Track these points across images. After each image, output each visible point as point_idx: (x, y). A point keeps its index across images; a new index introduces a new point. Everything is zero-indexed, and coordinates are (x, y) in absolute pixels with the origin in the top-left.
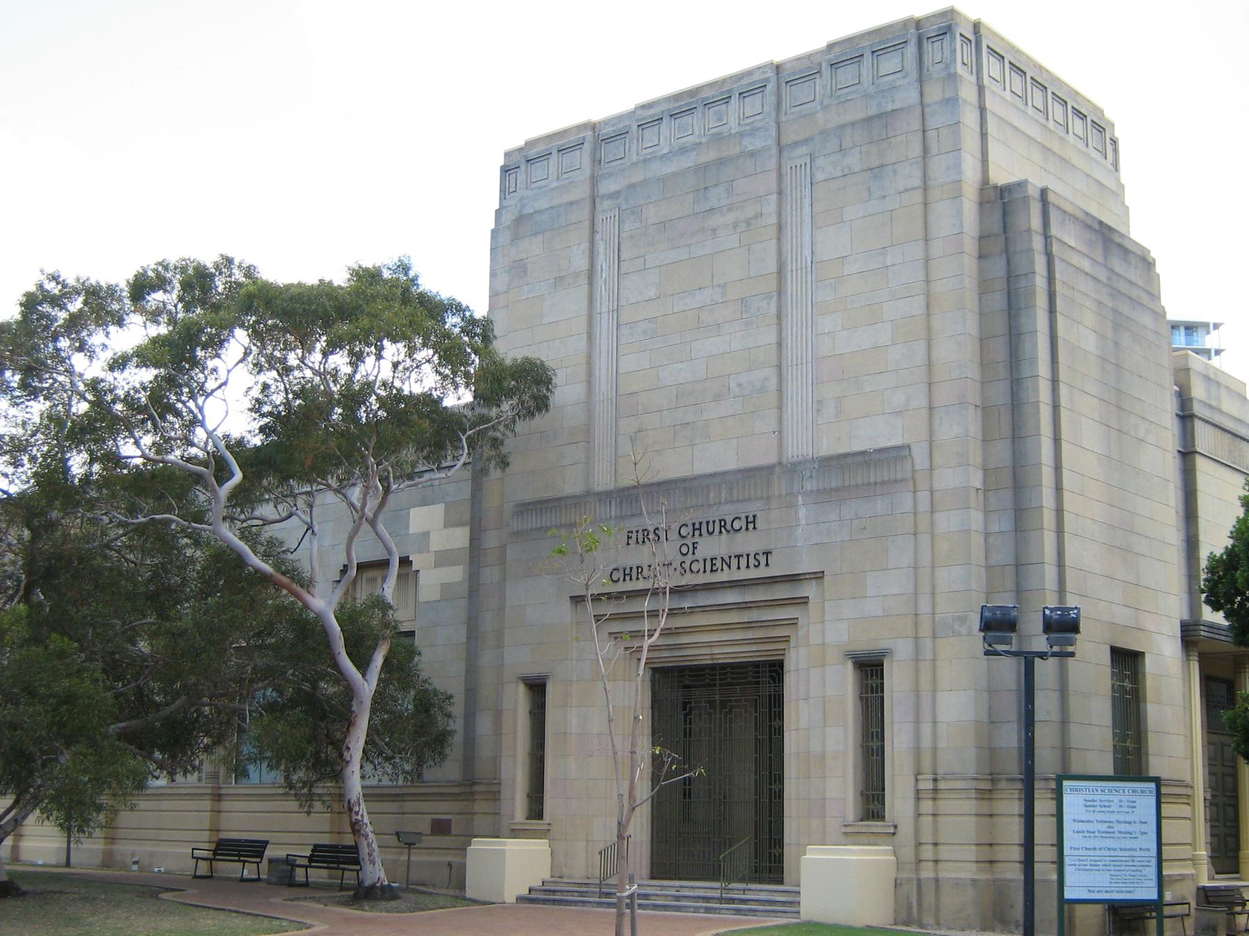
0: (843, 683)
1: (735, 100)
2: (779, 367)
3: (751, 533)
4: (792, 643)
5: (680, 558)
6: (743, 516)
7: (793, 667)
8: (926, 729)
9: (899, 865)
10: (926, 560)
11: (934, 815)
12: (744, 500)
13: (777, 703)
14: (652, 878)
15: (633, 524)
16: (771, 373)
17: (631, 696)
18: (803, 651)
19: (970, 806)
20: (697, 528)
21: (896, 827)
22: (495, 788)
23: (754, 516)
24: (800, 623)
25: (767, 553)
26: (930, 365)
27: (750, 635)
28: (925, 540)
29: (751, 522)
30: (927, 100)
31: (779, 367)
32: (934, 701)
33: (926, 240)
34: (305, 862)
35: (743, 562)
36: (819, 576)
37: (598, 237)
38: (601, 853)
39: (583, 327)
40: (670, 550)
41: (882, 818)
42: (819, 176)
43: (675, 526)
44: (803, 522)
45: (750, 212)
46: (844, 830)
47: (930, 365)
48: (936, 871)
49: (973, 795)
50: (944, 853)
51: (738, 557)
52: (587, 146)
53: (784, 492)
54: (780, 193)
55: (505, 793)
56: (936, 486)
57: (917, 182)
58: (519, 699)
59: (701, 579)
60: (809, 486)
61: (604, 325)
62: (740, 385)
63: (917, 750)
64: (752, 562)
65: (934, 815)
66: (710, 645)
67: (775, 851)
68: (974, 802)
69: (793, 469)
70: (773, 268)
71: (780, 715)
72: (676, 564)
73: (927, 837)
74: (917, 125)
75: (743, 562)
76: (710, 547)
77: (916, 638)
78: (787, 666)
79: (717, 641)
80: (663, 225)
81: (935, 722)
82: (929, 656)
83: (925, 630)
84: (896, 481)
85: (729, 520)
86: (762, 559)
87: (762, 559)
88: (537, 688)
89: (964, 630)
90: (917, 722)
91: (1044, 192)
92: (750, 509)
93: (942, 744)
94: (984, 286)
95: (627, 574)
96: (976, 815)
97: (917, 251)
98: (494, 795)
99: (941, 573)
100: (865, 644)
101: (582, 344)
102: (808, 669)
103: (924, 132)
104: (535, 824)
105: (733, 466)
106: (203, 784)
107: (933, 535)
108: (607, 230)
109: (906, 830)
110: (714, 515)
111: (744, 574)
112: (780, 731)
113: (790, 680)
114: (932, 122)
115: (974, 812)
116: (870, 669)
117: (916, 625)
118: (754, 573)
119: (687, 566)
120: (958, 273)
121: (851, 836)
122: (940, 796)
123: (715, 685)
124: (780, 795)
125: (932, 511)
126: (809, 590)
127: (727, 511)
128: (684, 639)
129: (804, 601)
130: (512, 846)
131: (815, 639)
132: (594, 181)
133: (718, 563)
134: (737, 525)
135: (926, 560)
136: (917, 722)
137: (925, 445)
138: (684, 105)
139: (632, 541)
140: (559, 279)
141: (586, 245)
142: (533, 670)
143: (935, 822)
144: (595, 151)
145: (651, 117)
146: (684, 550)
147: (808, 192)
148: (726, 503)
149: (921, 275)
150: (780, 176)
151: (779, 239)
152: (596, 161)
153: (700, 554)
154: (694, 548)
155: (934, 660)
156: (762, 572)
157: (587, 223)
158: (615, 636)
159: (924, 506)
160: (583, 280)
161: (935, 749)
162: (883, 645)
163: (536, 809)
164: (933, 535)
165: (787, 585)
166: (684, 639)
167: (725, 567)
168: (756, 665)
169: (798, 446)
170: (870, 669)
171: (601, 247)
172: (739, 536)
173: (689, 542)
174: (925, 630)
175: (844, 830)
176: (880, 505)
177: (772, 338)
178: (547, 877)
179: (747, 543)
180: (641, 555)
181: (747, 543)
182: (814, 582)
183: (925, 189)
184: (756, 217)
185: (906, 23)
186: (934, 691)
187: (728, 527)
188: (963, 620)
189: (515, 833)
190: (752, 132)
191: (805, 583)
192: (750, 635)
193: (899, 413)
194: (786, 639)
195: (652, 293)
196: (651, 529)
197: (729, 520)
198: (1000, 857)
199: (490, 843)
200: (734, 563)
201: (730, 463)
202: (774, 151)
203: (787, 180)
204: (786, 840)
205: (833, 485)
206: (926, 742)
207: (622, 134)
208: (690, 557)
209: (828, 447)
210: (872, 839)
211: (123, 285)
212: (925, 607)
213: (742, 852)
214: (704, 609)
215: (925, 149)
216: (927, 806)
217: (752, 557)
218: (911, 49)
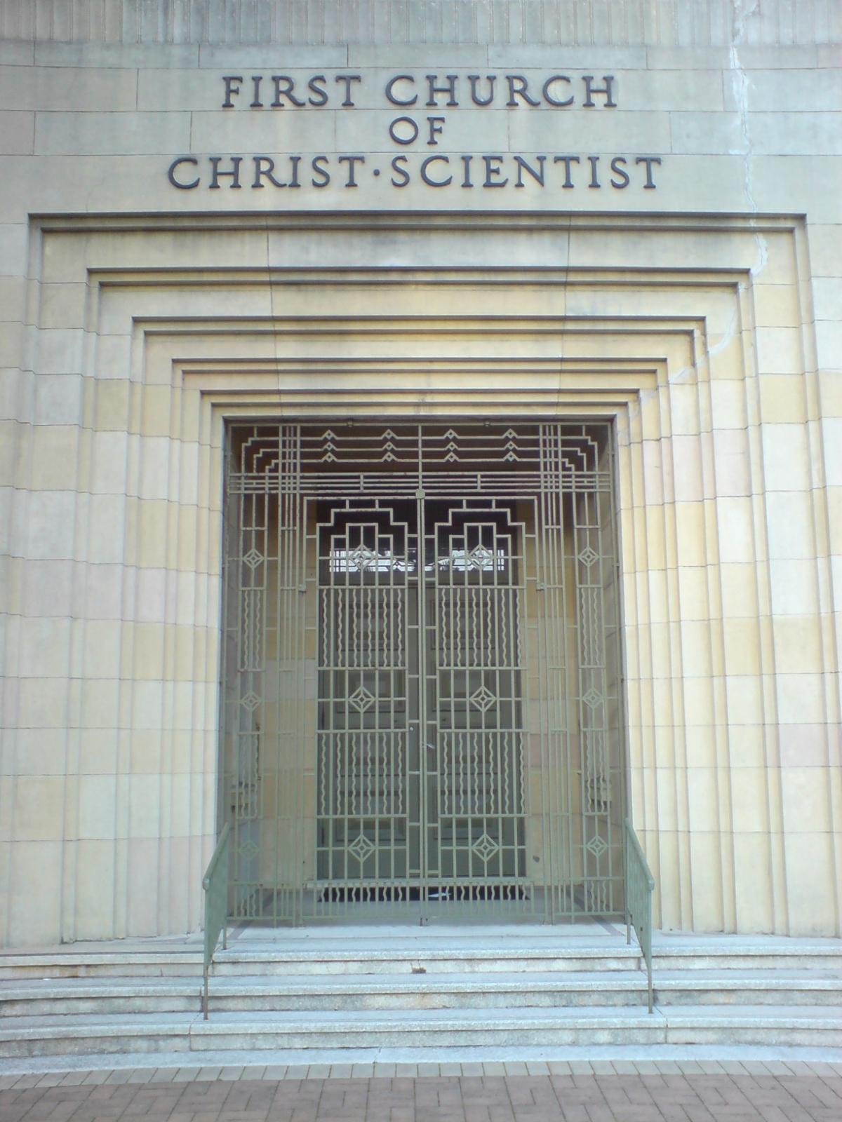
3: (600, 115)
6: (576, 76)
12: (577, 44)
17: (187, 475)
23: (608, 80)
25: (649, 161)
27: (554, 348)
36: (789, 225)
40: (363, 130)
44: (744, 105)
48: (206, 985)
51: (567, 160)
53: (685, 39)
59: (453, 199)
60: (753, 32)
66: (427, 366)
75: (581, 174)
76: (468, 132)
79: (437, 356)
92: (599, 63)
95: (225, 170)
106: (193, 937)
111: (581, 200)
123: (414, 467)
126: (752, 254)
131: (776, 352)
133: (508, 171)
139: (242, 100)
146: (404, 131)
148: (524, 42)
153: (445, 144)
154: (433, 131)
156: (634, 200)
167: (527, 178)
168: (528, 427)
172: (565, 116)
175: (294, 891)
179: (575, 131)
181: (575, 131)
191: (737, 239)
192: (554, 348)
197: (535, 80)
200: (554, 174)
205: (821, 35)
208: (421, 149)
214: (439, 277)
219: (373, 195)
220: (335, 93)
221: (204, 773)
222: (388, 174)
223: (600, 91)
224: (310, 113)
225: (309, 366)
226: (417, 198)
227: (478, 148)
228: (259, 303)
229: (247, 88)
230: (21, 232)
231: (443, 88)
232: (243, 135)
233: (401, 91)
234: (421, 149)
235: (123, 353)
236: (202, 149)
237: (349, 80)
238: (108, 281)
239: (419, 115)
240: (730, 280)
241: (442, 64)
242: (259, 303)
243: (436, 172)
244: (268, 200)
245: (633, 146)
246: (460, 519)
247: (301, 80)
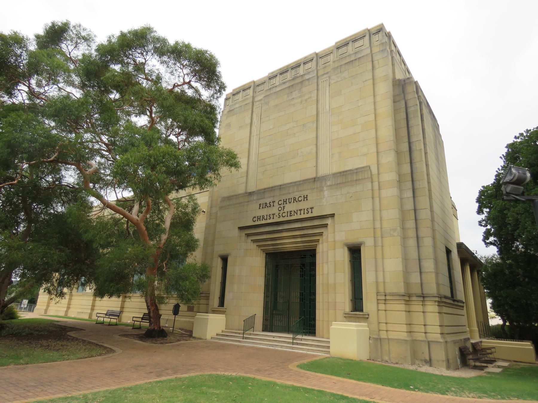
0: (344, 256)
1: (302, 66)
2: (317, 145)
3: (306, 201)
4: (320, 242)
5: (279, 212)
6: (302, 196)
7: (321, 251)
8: (380, 274)
9: (371, 332)
10: (377, 207)
11: (385, 310)
13: (313, 265)
14: (263, 331)
15: (262, 201)
16: (314, 147)
18: (325, 244)
19: (402, 307)
20: (285, 201)
21: (368, 315)
22: (208, 295)
24: (324, 234)
25: (312, 208)
26: (377, 138)
28: (377, 200)
29: (306, 198)
30: (373, 52)
31: (317, 145)
32: (383, 263)
33: (374, 96)
34: (140, 320)
35: (302, 212)
36: (332, 216)
37: (254, 113)
38: (244, 321)
39: (248, 141)
40: (275, 210)
41: (362, 310)
42: (332, 82)
43: (277, 202)
44: (326, 196)
45: (306, 97)
46: (345, 315)
47: (377, 138)
49: (437, 304)
50: (390, 327)
51: (300, 210)
52: (252, 88)
54: (318, 90)
55: (211, 297)
56: (381, 180)
57: (371, 77)
58: (219, 263)
59: (286, 219)
61: (254, 140)
62: (302, 152)
63: (377, 282)
64: (306, 211)
65: (385, 310)
67: (312, 323)
68: (404, 305)
69: (324, 178)
70: (315, 113)
71: (315, 270)
72: (277, 214)
73: (383, 320)
74: (370, 59)
75: (302, 212)
76: (289, 207)
77: (375, 237)
78: (317, 251)
79: (289, 243)
80: (277, 105)
81: (384, 271)
82: (380, 245)
83: (379, 234)
84: (365, 178)
85: (297, 197)
86: (310, 210)
87: (310, 210)
88: (225, 260)
89: (395, 234)
90: (376, 271)
91: (217, 334)
92: (305, 193)
93: (387, 280)
94: (396, 111)
95: (259, 218)
96: (405, 311)
97: (371, 100)
98: (208, 298)
99: (385, 213)
100: (353, 239)
101: (247, 146)
102: (327, 251)
103: (372, 62)
104: (221, 309)
105: (299, 179)
107: (380, 198)
108: (256, 110)
109: (373, 317)
110: (291, 196)
111: (303, 216)
112: (315, 276)
113: (318, 256)
114: (375, 58)
115: (404, 310)
116: (355, 252)
117: (374, 232)
118: (306, 216)
119: (281, 215)
120: (385, 106)
121: (348, 317)
122: (426, 303)
124: (314, 300)
125: (380, 189)
126: (329, 221)
127: (297, 195)
128: (278, 242)
129: (326, 226)
130: (212, 317)
131: (331, 239)
132: (253, 97)
133: (293, 213)
134: (300, 199)
135: (377, 207)
136: (376, 271)
137: (376, 165)
138: (283, 71)
139: (261, 207)
140: (241, 127)
141: (250, 116)
142: (224, 253)
143: (386, 314)
144: (254, 89)
145: (272, 77)
146: (280, 209)
147: (328, 89)
148: (296, 192)
149: (373, 107)
150: (318, 85)
151: (317, 104)
152: (254, 92)
153: (286, 210)
155: (382, 246)
156: (310, 215)
157: (251, 110)
158: (254, 241)
159: (376, 187)
160: (249, 126)
161: (384, 282)
162: (360, 240)
163: (222, 303)
164: (380, 198)
165: (319, 220)
166: (278, 242)
169: (324, 170)
170: (355, 252)
171: (254, 115)
172: (301, 203)
173: (282, 206)
174: (379, 234)
176: (359, 188)
177: (315, 135)
178: (224, 329)
179: (304, 205)
180: (264, 212)
181: (304, 205)
182: (330, 218)
183: (373, 79)
184: (309, 98)
185: (364, 31)
186: (383, 258)
187: (297, 200)
188: (395, 230)
189: (214, 312)
190: (309, 73)
192: (304, 239)
193: (364, 155)
194: (318, 241)
195: (271, 127)
196: (268, 203)
197: (297, 197)
198: (415, 330)
199: (203, 315)
200: (299, 212)
201: (297, 178)
202: (316, 77)
203: (320, 86)
204: (317, 318)
206: (381, 279)
207: (263, 83)
208: (282, 211)
209: (335, 170)
210: (357, 319)
211: (32, 37)
212: (378, 225)
213: (295, 320)
215: (373, 68)
216: (382, 307)
217: (306, 210)
218: (367, 38)
219: (276, 220)
220: (272, 204)
221: (323, 321)
222: (278, 216)
223: (306, 198)
224: (269, 208)
225: (273, 245)
226: (282, 219)
227: (289, 210)
228: (265, 237)
229: (262, 205)
230: (237, 229)
231: (285, 201)
232: (264, 212)
233: (280, 203)
234: (282, 211)
235: (253, 246)
236: (256, 216)
237: (274, 202)
238: (248, 235)
239: (282, 206)
240: (326, 226)
241: (285, 197)
242: (265, 237)
243: (284, 215)
244: (264, 222)
245: (309, 206)
246: (303, 269)
247: (268, 203)
